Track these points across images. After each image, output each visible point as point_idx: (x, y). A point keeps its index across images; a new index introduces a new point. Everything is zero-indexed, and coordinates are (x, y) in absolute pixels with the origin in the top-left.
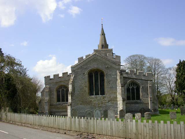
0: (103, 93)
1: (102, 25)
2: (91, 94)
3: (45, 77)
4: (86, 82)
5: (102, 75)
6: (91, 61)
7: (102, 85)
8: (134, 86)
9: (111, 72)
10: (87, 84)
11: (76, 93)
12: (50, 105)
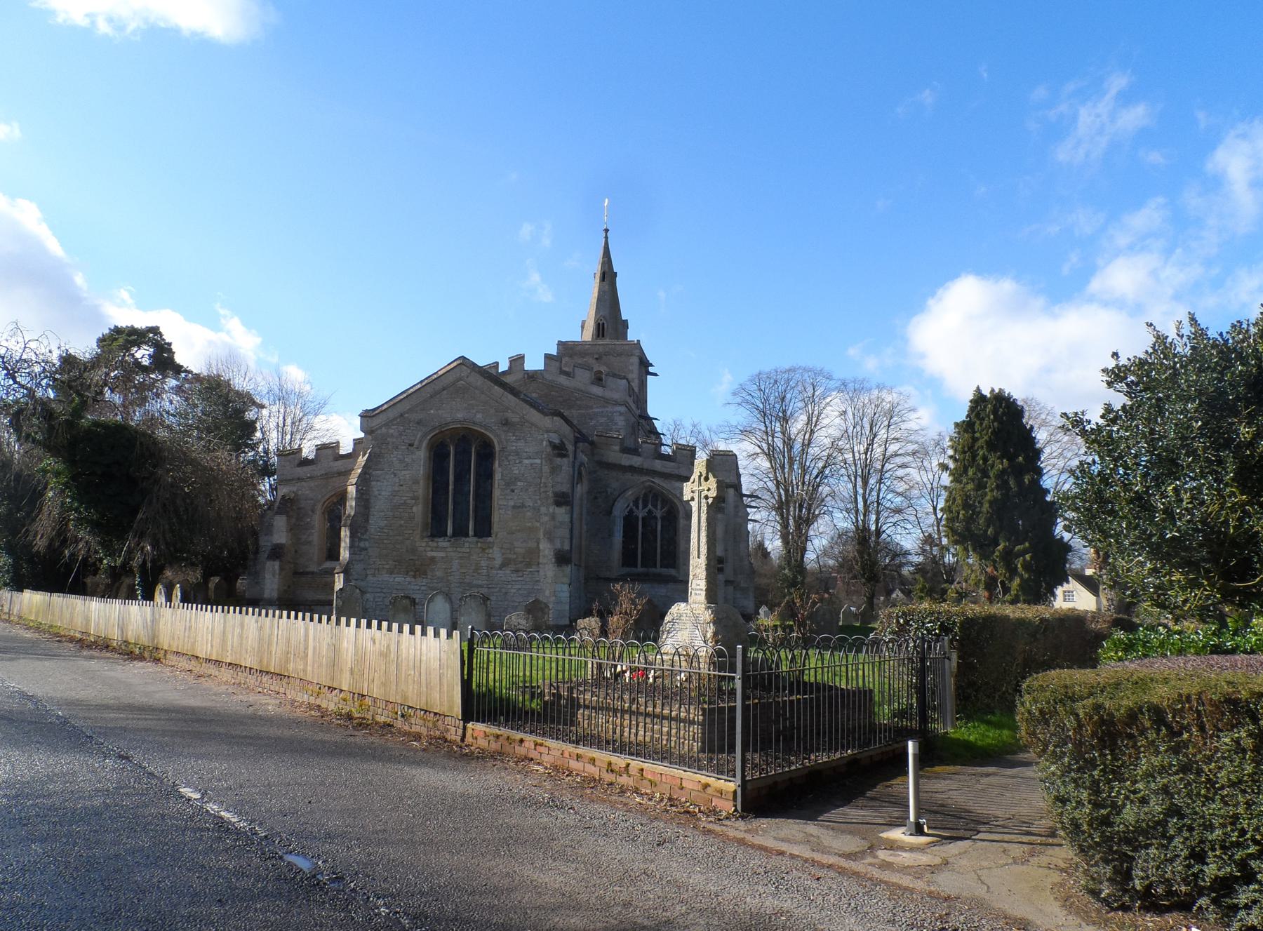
0: (484, 529)
1: (607, 231)
2: (436, 528)
3: (354, 440)
4: (416, 482)
5: (487, 453)
6: (445, 392)
7: (485, 498)
8: (655, 506)
9: (521, 444)
10: (422, 490)
11: (376, 521)
12: (296, 573)
